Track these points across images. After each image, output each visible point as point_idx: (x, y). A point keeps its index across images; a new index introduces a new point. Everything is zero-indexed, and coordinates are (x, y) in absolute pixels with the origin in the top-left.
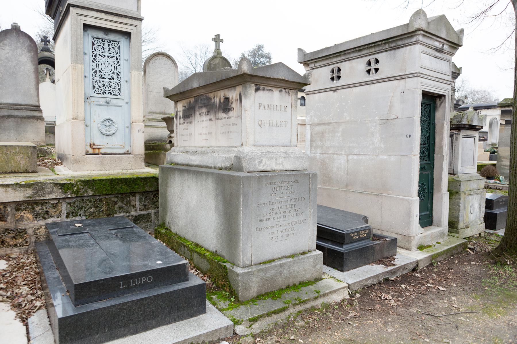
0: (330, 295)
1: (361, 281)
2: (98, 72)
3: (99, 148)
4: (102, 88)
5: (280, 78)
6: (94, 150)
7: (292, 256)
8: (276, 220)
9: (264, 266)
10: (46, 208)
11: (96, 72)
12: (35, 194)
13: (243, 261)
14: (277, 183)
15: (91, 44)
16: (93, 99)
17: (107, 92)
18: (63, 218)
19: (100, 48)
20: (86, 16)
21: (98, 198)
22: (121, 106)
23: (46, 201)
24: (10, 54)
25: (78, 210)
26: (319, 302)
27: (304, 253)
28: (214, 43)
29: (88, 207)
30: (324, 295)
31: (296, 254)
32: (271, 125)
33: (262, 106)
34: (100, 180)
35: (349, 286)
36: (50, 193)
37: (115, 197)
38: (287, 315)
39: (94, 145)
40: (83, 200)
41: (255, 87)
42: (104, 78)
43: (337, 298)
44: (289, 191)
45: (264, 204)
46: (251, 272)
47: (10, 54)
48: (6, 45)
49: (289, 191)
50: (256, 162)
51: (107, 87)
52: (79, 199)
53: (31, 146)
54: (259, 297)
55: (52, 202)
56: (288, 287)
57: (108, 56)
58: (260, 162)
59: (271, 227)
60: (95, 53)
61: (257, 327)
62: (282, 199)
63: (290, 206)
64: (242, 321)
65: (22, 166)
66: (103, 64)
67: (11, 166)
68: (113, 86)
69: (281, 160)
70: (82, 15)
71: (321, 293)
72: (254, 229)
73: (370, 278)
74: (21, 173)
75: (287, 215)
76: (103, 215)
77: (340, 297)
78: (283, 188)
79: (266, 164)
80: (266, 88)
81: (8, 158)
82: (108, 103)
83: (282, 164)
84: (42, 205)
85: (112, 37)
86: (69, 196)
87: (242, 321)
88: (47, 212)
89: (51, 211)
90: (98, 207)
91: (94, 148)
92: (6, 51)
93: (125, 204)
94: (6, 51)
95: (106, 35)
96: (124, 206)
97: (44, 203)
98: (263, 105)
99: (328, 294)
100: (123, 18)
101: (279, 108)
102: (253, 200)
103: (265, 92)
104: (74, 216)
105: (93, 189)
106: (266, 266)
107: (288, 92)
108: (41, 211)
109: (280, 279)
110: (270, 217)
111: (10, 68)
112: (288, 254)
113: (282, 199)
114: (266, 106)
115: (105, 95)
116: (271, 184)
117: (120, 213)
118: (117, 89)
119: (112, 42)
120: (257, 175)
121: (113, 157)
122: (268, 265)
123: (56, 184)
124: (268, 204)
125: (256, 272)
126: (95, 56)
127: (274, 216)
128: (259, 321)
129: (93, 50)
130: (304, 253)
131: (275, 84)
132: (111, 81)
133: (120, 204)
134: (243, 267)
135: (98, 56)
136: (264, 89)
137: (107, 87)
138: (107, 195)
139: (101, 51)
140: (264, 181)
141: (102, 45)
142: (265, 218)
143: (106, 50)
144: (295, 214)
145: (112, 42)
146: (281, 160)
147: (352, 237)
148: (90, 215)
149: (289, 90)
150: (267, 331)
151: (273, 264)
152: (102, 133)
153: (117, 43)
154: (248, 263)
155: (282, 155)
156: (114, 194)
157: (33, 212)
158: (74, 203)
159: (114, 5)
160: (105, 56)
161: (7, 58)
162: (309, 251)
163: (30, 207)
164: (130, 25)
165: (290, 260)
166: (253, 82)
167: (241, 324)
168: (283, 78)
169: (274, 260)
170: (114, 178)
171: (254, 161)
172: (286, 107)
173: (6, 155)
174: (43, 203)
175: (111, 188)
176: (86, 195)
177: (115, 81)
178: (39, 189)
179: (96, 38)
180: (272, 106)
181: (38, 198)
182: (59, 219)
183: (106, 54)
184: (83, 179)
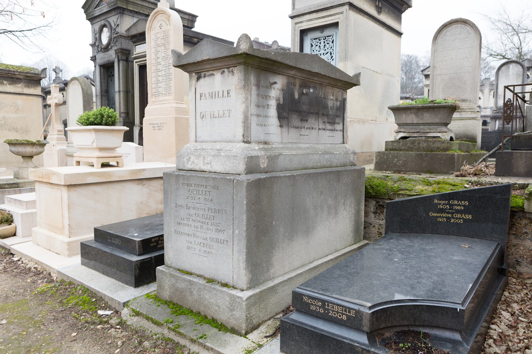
5: (205, 58)
7: (211, 281)
8: (193, 228)
9: (178, 274)
15: (310, 46)
19: (317, 48)
20: (301, 22)
27: (225, 285)
28: (92, 62)
31: (216, 281)
32: (213, 116)
46: (164, 272)
50: (185, 160)
58: (189, 160)
62: (198, 205)
69: (209, 159)
72: (173, 230)
75: (205, 226)
78: (200, 193)
79: (193, 162)
85: (327, 32)
95: (322, 32)
98: (204, 94)
100: (331, 10)
112: (207, 276)
113: (198, 205)
116: (188, 185)
119: (327, 38)
127: (190, 222)
130: (225, 285)
131: (211, 66)
136: (205, 76)
140: (181, 181)
141: (318, 44)
143: (322, 47)
144: (214, 228)
145: (327, 38)
146: (209, 159)
153: (331, 37)
164: (337, 14)
165: (202, 282)
168: (208, 58)
169: (191, 274)
171: (183, 158)
179: (315, 39)
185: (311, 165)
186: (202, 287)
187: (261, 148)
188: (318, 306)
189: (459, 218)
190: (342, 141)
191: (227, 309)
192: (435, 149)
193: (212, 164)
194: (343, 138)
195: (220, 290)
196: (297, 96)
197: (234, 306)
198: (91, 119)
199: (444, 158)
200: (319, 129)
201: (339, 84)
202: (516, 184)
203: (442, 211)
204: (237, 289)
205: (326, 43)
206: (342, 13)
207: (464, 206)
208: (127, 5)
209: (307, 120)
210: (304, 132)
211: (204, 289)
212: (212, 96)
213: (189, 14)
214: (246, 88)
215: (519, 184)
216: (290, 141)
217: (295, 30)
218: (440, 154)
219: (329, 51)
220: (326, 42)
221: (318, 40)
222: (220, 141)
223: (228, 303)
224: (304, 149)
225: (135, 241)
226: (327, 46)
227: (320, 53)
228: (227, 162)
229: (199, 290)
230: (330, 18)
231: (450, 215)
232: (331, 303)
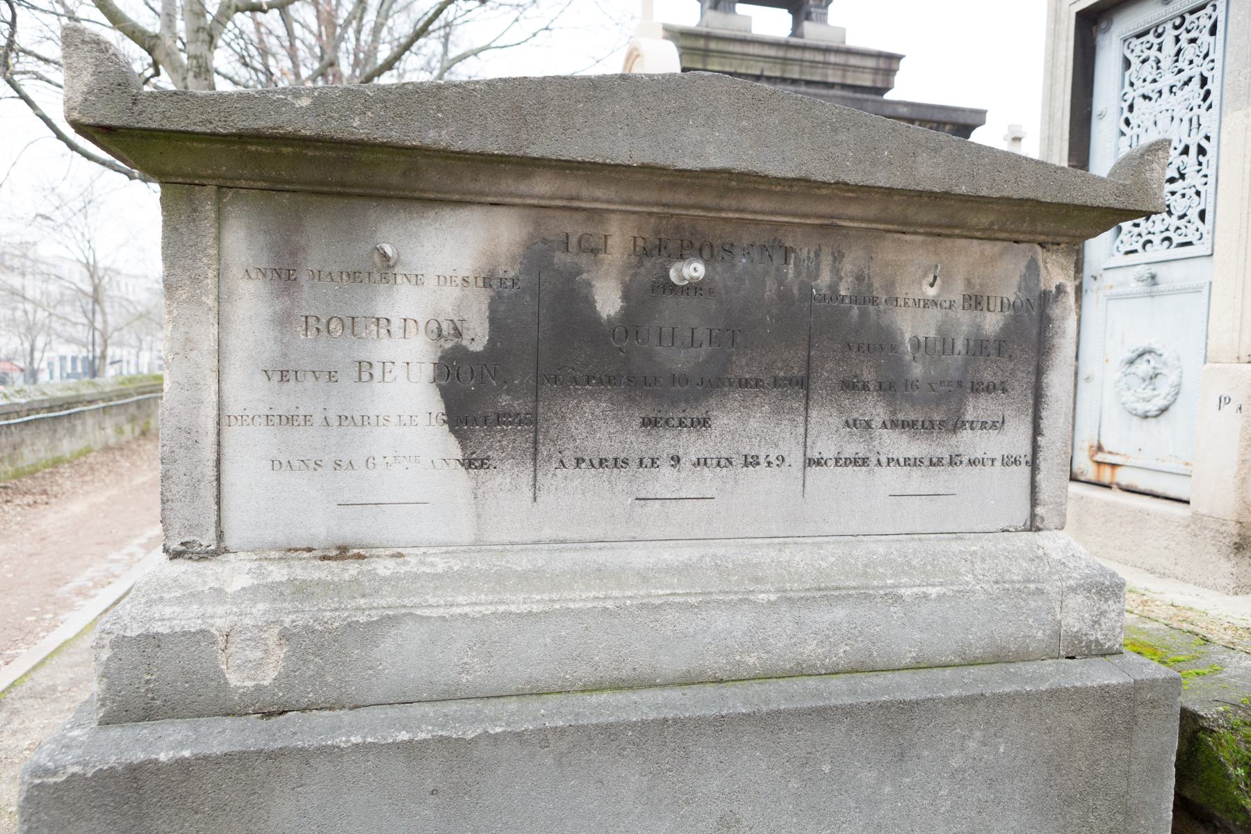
15: (1119, 64)
16: (1110, 277)
17: (1157, 239)
119: (1189, 18)
126: (1131, 108)
131: (693, 200)
141: (1153, 53)
143: (1166, 63)
160: (1160, 92)
179: (1138, 36)
185: (672, 663)
187: (273, 586)
190: (1021, 514)
194: (1034, 502)
196: (608, 301)
198: (78, 422)
200: (811, 462)
201: (984, 220)
205: (1183, 43)
208: (704, 63)
209: (704, 423)
210: (665, 480)
213: (879, 55)
214: (182, 294)
216: (547, 533)
219: (1195, 72)
220: (1185, 37)
221: (1150, 37)
224: (644, 577)
226: (1189, 51)
227: (1157, 86)
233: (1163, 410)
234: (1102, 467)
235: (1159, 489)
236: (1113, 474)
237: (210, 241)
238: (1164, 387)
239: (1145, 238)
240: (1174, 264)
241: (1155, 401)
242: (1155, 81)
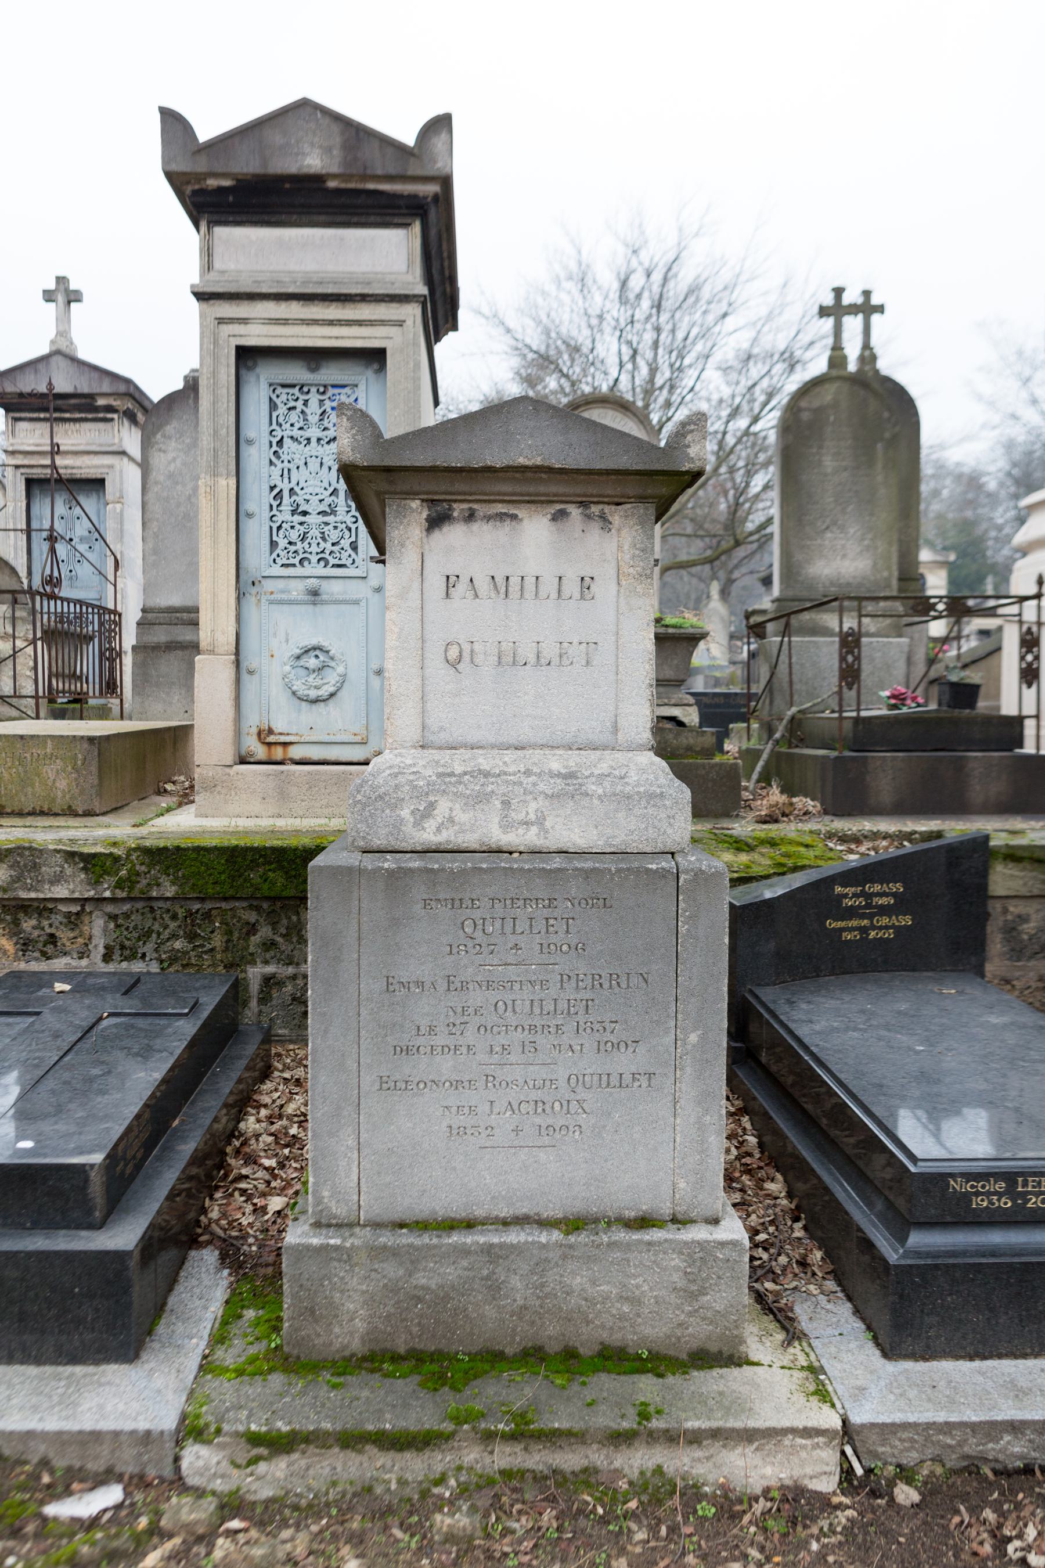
0: (715, 1447)
1: (948, 1427)
2: (286, 494)
3: (285, 744)
4: (299, 546)
5: (522, 461)
6: (272, 751)
8: (482, 1057)
9: (405, 1238)
10: (51, 926)
11: (279, 496)
12: (14, 882)
13: (319, 1201)
14: (486, 903)
15: (265, 407)
16: (269, 585)
17: (314, 559)
18: (95, 961)
20: (244, 321)
21: (196, 906)
22: (356, 602)
23: (50, 906)
24: (178, 462)
25: (139, 939)
26: (636, 1461)
27: (644, 1222)
29: (166, 934)
30: (671, 1438)
31: (596, 1221)
32: (508, 660)
33: (462, 586)
34: (198, 849)
35: (848, 1431)
36: (56, 880)
37: (251, 907)
38: (439, 1468)
39: (271, 732)
40: (152, 910)
41: (425, 514)
42: (305, 513)
43: (753, 1471)
44: (553, 938)
45: (420, 984)
46: (336, 1248)
47: (178, 462)
48: (170, 438)
49: (553, 938)
50: (405, 813)
51: (314, 542)
52: (140, 905)
53: (82, 737)
54: (374, 1360)
55: (63, 908)
56: (533, 1356)
57: (319, 440)
58: (428, 812)
59: (456, 1084)
60: (279, 434)
61: (271, 1477)
63: (562, 1005)
64: (218, 1432)
65: (59, 793)
66: (302, 467)
67: (33, 794)
68: (334, 536)
69: (533, 806)
70: (231, 321)
71: (655, 1424)
72: (368, 1080)
73: (1015, 1427)
74: (56, 815)
76: (214, 965)
77: (768, 1471)
79: (451, 820)
80: (481, 509)
81: (26, 772)
82: (315, 593)
83: (540, 821)
84: (40, 915)
85: (330, 373)
86: (107, 894)
87: (218, 1432)
88: (52, 939)
89: (64, 935)
90: (196, 936)
91: (269, 744)
92: (171, 455)
93: (283, 936)
94: (171, 455)
95: (313, 370)
96: (279, 939)
97: (45, 909)
98: (464, 580)
99: (695, 1438)
101: (549, 586)
102: (364, 962)
103: (475, 526)
104: (126, 959)
105: (177, 878)
106: (418, 1242)
107: (603, 517)
108: (36, 933)
109: (490, 1311)
110: (450, 1041)
111: (178, 505)
112: (552, 1210)
114: (483, 585)
115: (308, 570)
116: (456, 904)
117: (266, 962)
118: (347, 546)
120: (389, 863)
121: (318, 773)
122: (426, 1239)
123: (71, 856)
124: (442, 986)
125: (363, 1255)
126: (280, 443)
128: (295, 1456)
129: (274, 426)
130: (644, 1222)
131: (518, 489)
132: (326, 519)
133: (265, 932)
134: (317, 1225)
135: (287, 442)
137: (314, 542)
138: (225, 899)
139: (297, 425)
140: (419, 891)
141: (299, 405)
142: (420, 1041)
143: (313, 419)
144: (588, 1041)
146: (533, 806)
147: (966, 1197)
148: (173, 960)
149: (607, 509)
150: (304, 1502)
151: (455, 1238)
152: (294, 693)
154: (340, 1210)
155: (542, 787)
156: (246, 899)
157: (15, 934)
158: (127, 916)
159: (330, 268)
160: (309, 439)
161: (171, 476)
162: (674, 1220)
163: (8, 918)
164: (382, 323)
165: (556, 1235)
166: (411, 494)
167: (209, 1442)
168: (539, 461)
169: (469, 1224)
170: (242, 843)
171: (394, 807)
172: (585, 583)
173: (22, 761)
174: (43, 908)
175: (233, 878)
176: (154, 894)
177: (339, 518)
178: (25, 865)
179: (284, 386)
180: (514, 581)
181: (23, 895)
182: (84, 962)
183: (314, 432)
184: (147, 843)
186: (554, 1255)
188: (996, 1193)
189: (884, 928)
191: (673, 1299)
192: (681, 752)
193: (548, 824)
195: (640, 1242)
197: (709, 1277)
199: (713, 775)
202: (916, 832)
203: (852, 913)
204: (692, 1221)
206: (400, 324)
207: (894, 895)
211: (564, 1257)
212: (503, 587)
215: (921, 833)
217: (216, 343)
218: (703, 766)
221: (296, 391)
222: (542, 746)
223: (676, 1277)
225: (81, 1170)
228: (621, 815)
229: (541, 1266)
230: (355, 331)
231: (865, 922)
232: (1035, 1174)
233: (332, 695)
234: (273, 748)
235: (343, 759)
236: (285, 752)
237: (191, 401)
238: (331, 679)
239: (301, 556)
240: (333, 581)
241: (325, 688)
242: (301, 429)
